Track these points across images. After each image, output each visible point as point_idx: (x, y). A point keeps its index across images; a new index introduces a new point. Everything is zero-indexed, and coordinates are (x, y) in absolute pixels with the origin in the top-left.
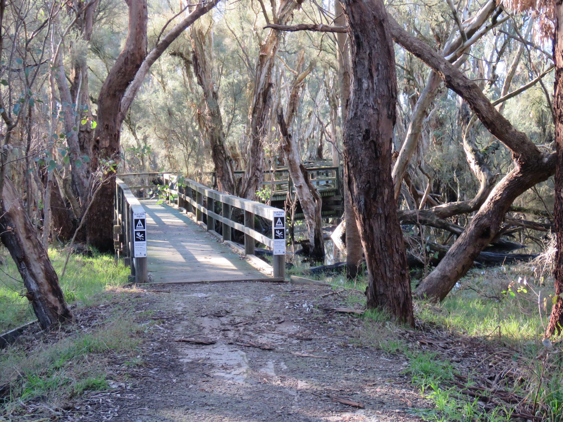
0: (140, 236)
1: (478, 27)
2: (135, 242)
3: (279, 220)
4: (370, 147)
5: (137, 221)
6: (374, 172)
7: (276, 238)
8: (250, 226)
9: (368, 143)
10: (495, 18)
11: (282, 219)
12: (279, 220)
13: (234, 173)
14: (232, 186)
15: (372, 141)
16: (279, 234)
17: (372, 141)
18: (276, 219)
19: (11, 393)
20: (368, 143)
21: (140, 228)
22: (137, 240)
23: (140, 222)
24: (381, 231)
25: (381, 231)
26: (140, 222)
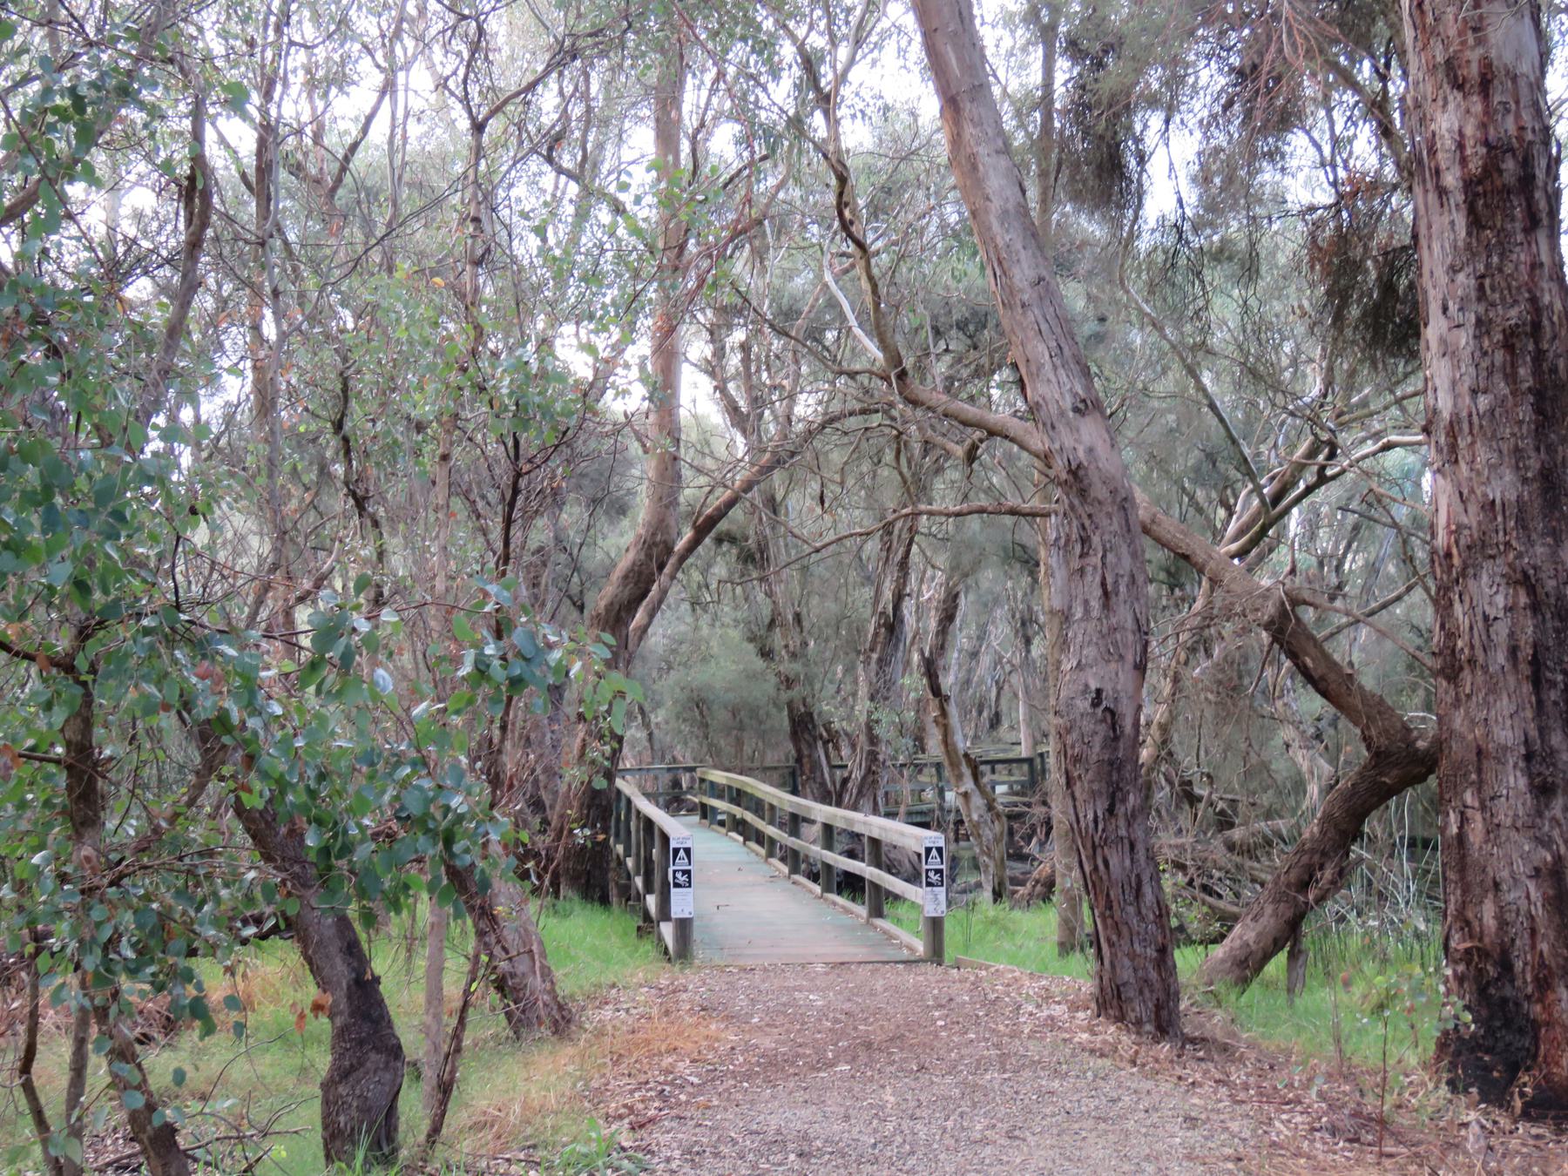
0: (681, 879)
1: (1295, 484)
2: (673, 890)
3: (934, 852)
4: (1103, 720)
5: (676, 851)
6: (1111, 763)
7: (929, 884)
8: (713, 796)
9: (1099, 711)
10: (1323, 468)
11: (939, 850)
12: (934, 852)
13: (832, 767)
14: (829, 793)
15: (1107, 709)
16: (934, 878)
17: (1107, 709)
18: (928, 850)
19: (677, 828)
20: (1099, 711)
21: (681, 864)
22: (677, 885)
23: (682, 853)
24: (1124, 869)
25: (1124, 869)
26: (682, 853)
